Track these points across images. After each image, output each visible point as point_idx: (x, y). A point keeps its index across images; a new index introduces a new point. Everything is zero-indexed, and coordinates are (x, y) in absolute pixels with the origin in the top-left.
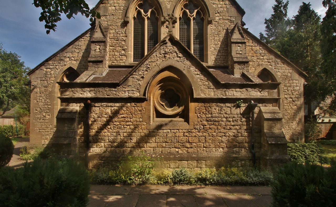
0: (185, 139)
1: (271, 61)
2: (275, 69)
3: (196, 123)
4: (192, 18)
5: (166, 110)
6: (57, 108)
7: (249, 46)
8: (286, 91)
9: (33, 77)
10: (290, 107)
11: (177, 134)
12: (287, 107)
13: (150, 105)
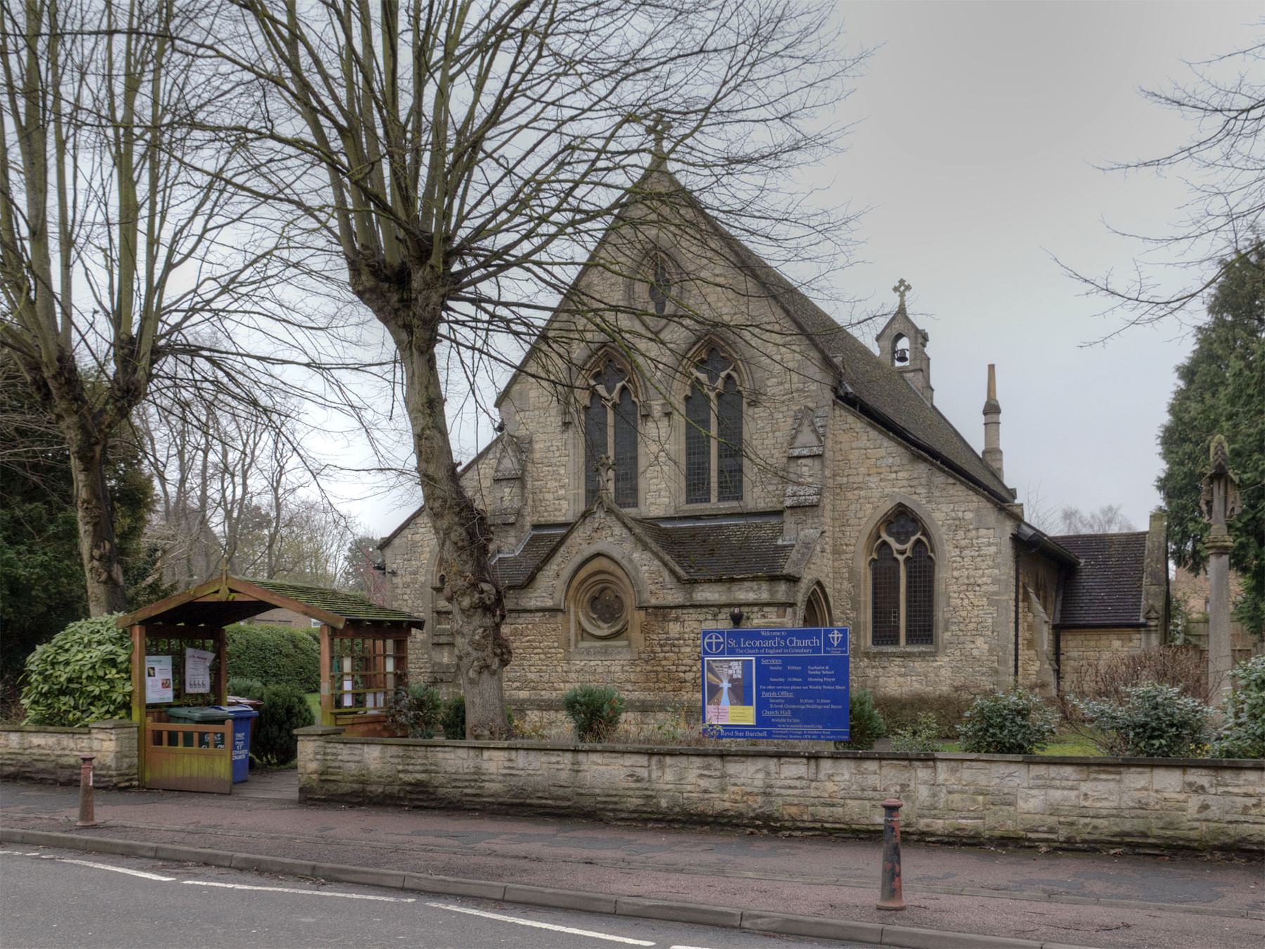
0: (623, 677)
1: (915, 483)
2: (929, 502)
3: (641, 649)
4: (712, 395)
5: (599, 627)
6: (1020, 597)
7: (860, 448)
8: (958, 559)
9: (388, 552)
10: (966, 601)
11: (613, 669)
12: (959, 602)
13: (568, 621)
